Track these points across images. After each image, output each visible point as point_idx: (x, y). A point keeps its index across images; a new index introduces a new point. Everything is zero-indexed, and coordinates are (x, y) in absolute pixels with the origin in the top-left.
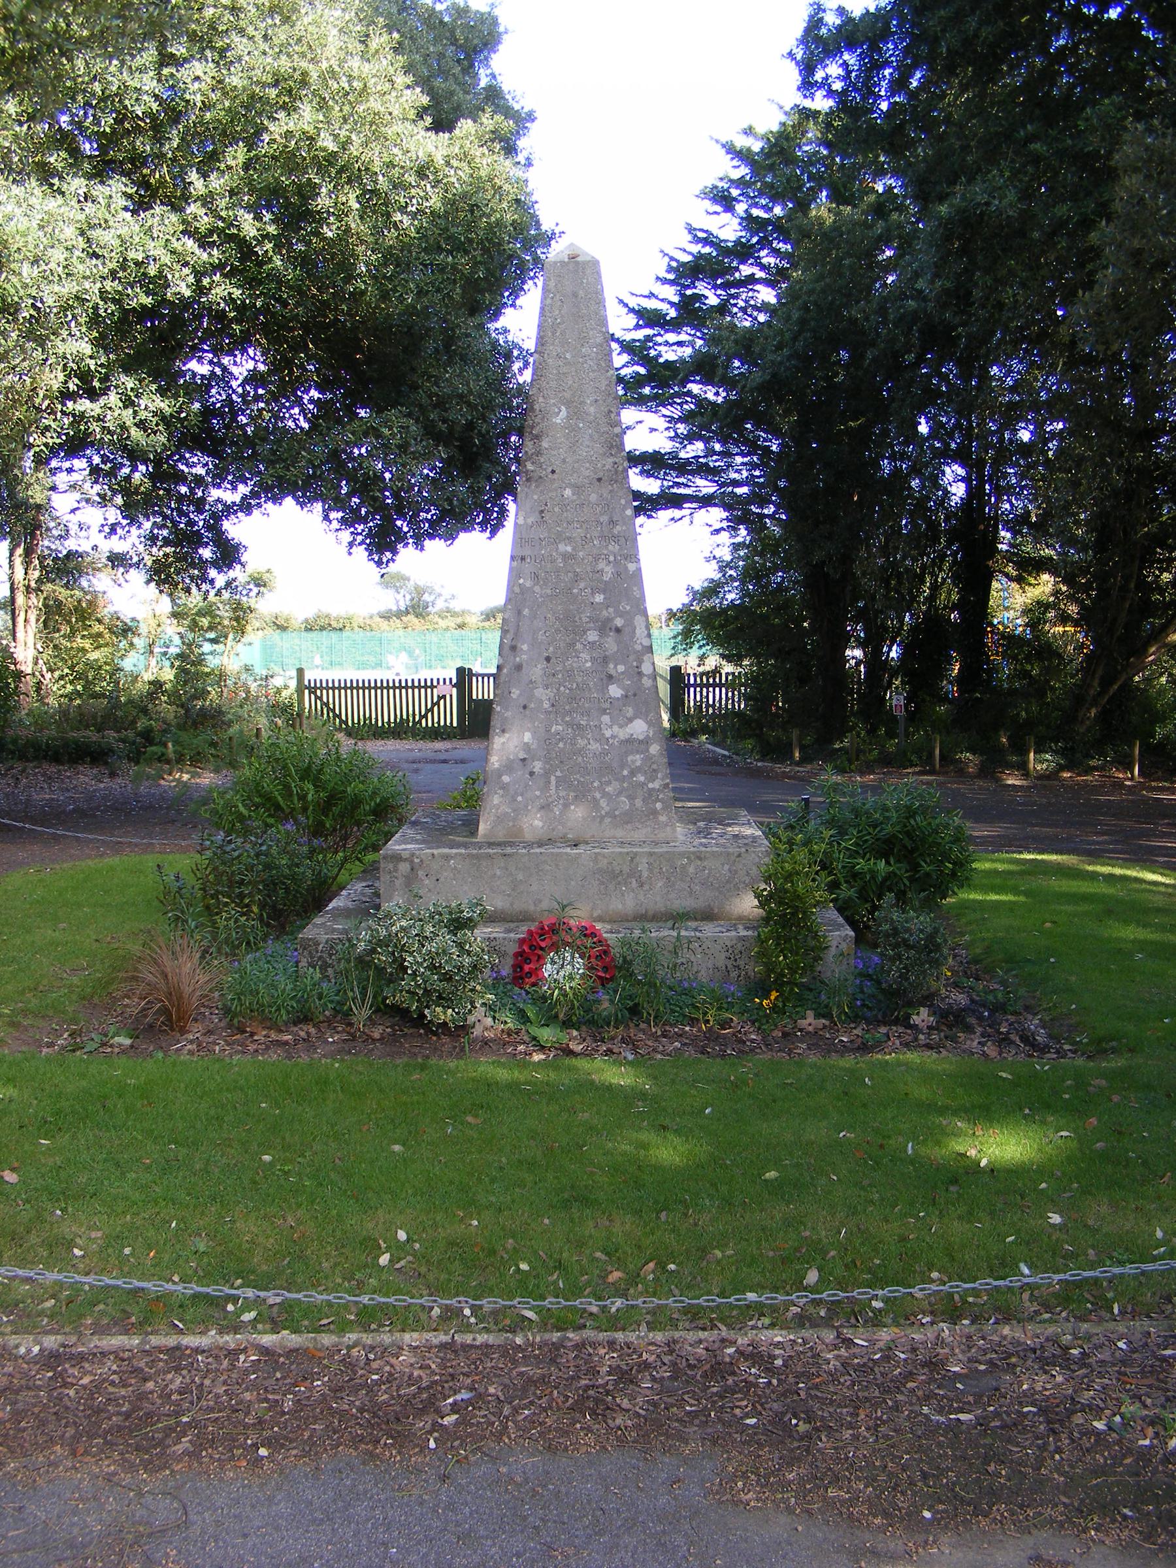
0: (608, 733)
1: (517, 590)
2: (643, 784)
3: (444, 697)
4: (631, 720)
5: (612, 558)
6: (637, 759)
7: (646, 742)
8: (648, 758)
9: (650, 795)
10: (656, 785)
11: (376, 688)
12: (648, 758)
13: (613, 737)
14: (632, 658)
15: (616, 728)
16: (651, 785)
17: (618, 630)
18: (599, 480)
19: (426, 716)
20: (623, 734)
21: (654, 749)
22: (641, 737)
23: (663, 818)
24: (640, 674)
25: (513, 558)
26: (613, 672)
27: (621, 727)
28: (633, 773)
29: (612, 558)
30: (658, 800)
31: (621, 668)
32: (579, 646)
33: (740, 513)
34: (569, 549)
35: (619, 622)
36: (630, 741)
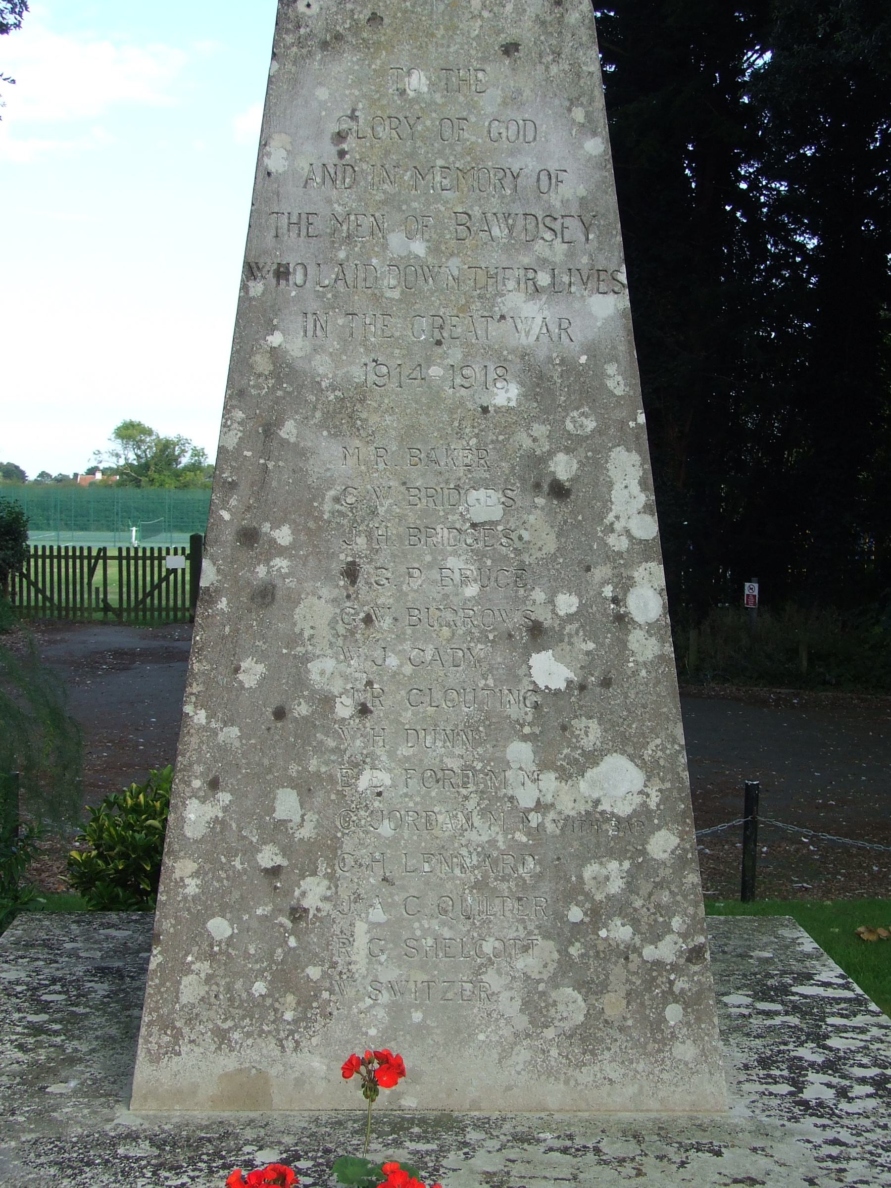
0: (526, 797)
1: (262, 364)
2: (626, 953)
3: (175, 571)
4: (593, 758)
5: (544, 279)
6: (609, 875)
7: (639, 823)
8: (642, 868)
9: (650, 983)
10: (666, 950)
11: (67, 557)
12: (642, 868)
13: (540, 807)
14: (601, 572)
15: (549, 780)
16: (649, 952)
17: (559, 491)
18: (510, 49)
19: (151, 593)
20: (571, 797)
21: (663, 844)
22: (624, 810)
23: (685, 1050)
24: (622, 620)
25: (251, 270)
26: (543, 616)
27: (564, 776)
28: (597, 915)
29: (544, 279)
30: (670, 996)
31: (567, 603)
32: (442, 534)
33: (522, 384)
34: (419, 248)
35: (563, 467)
36: (593, 819)
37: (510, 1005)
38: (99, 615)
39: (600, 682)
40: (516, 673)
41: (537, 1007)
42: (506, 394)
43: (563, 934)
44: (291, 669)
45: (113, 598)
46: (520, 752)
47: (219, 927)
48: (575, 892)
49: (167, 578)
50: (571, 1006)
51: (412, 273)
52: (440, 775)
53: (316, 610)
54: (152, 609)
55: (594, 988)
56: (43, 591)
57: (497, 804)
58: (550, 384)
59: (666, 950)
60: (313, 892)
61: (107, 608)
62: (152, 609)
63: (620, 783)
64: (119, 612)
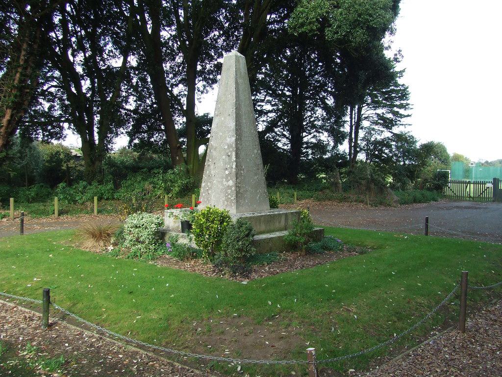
7: (232, 187)
10: (233, 198)
21: (233, 188)
37: (222, 203)
38: (468, 199)
39: (230, 173)
40: (225, 172)
41: (224, 203)
42: (226, 147)
43: (226, 196)
44: (210, 172)
45: (472, 195)
46: (224, 180)
47: (204, 194)
48: (227, 193)
49: (487, 190)
50: (226, 203)
51: (221, 136)
52: (219, 182)
53: (212, 167)
54: (482, 198)
55: (227, 201)
56: (454, 192)
57: (222, 185)
58: (229, 146)
59: (233, 198)
60: (210, 192)
61: (470, 197)
62: (482, 198)
63: (231, 183)
64: (473, 198)
